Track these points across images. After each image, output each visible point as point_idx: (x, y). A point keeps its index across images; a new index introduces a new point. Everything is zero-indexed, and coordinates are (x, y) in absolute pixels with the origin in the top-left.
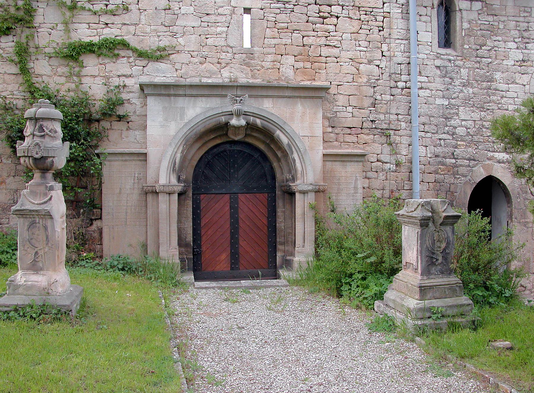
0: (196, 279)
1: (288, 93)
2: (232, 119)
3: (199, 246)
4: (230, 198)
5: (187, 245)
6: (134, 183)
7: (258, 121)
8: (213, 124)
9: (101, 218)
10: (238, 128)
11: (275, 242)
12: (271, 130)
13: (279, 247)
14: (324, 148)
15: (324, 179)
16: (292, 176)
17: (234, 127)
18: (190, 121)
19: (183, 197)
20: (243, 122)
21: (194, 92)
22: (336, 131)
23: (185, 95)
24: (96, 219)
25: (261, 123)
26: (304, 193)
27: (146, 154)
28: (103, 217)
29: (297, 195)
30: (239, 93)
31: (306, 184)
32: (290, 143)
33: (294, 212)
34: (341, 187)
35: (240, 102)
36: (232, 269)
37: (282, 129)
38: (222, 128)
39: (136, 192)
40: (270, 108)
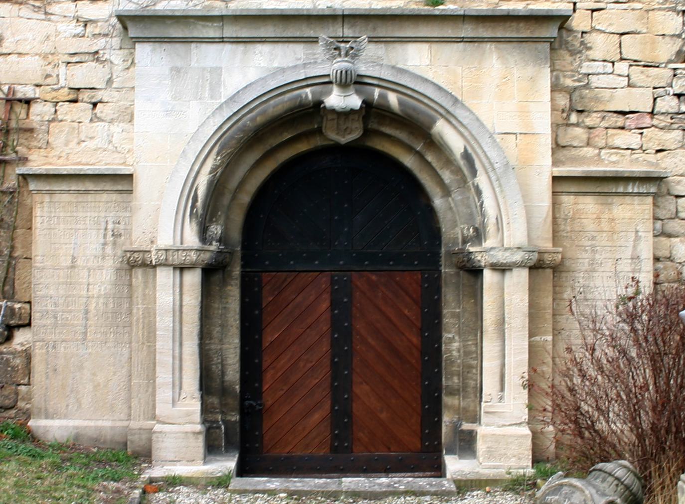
0: (243, 470)
1: (467, 31)
2: (329, 93)
3: (257, 394)
4: (333, 282)
5: (224, 391)
6: (105, 244)
7: (393, 99)
8: (287, 106)
9: (29, 325)
10: (347, 114)
11: (439, 389)
12: (422, 118)
13: (447, 400)
14: (555, 163)
15: (556, 236)
16: (476, 230)
17: (333, 111)
18: (232, 99)
19: (217, 278)
20: (355, 101)
21: (245, 32)
22: (589, 121)
23: (222, 40)
24: (19, 326)
25: (401, 103)
26: (502, 269)
27: (129, 177)
28: (33, 324)
29: (488, 276)
30: (348, 32)
31: (507, 249)
32: (470, 151)
33: (480, 318)
34: (597, 256)
35: (347, 55)
36: (334, 450)
37: (448, 117)
38: (306, 115)
39: (110, 264)
40: (421, 66)
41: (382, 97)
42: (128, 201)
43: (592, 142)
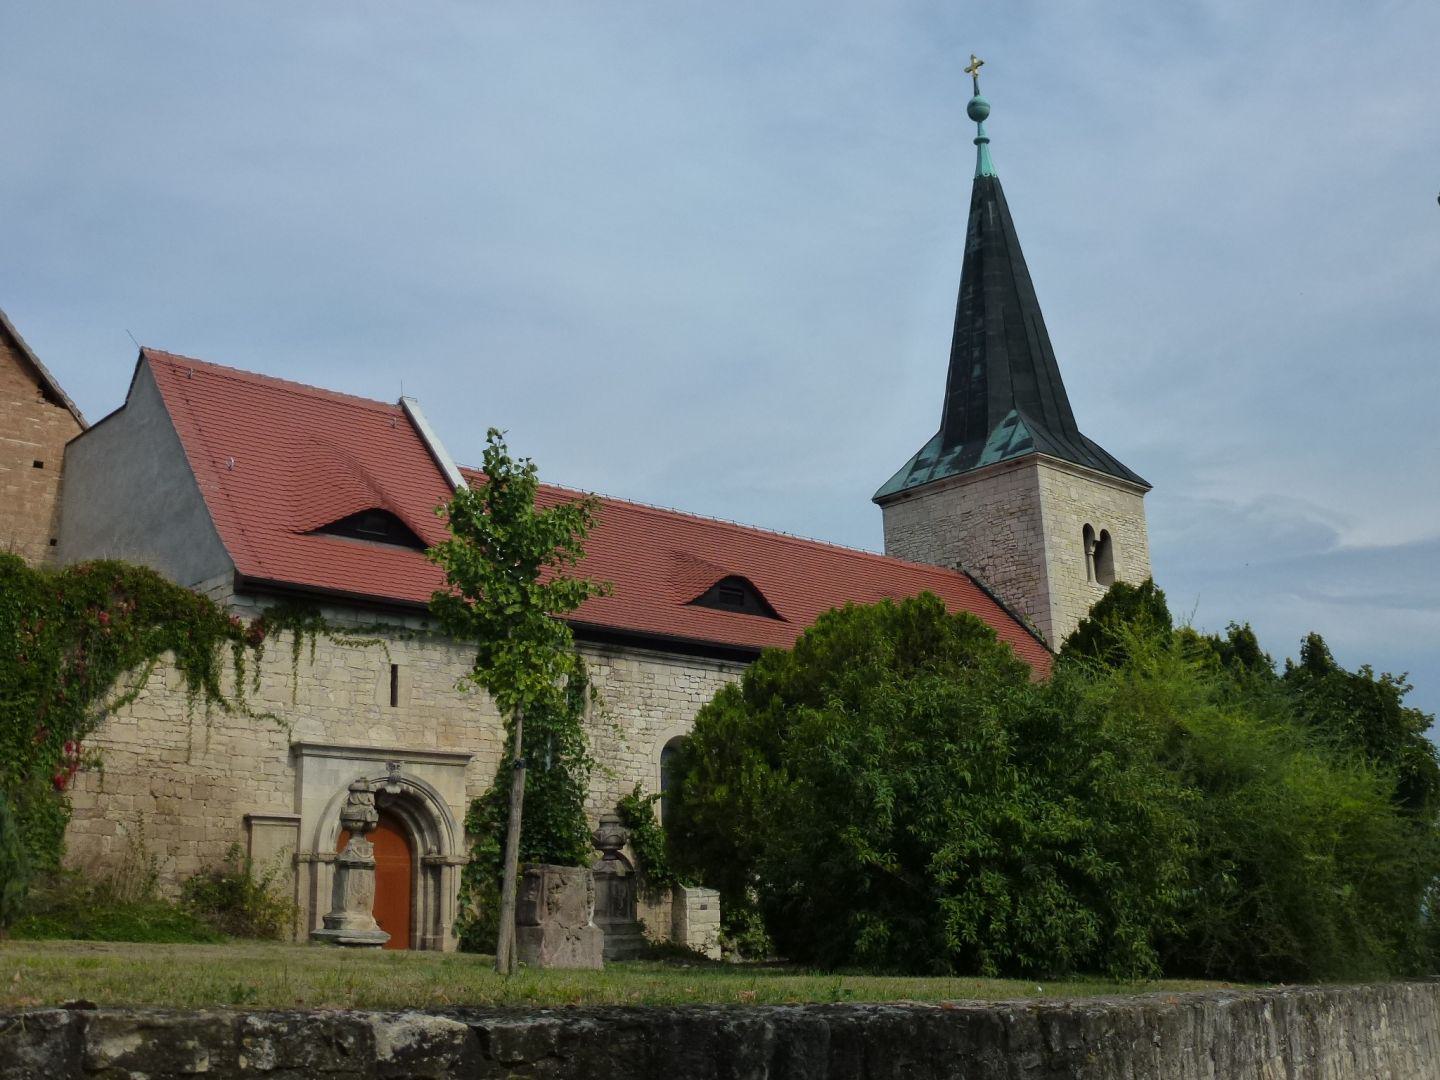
37: (433, 798)
41: (408, 788)
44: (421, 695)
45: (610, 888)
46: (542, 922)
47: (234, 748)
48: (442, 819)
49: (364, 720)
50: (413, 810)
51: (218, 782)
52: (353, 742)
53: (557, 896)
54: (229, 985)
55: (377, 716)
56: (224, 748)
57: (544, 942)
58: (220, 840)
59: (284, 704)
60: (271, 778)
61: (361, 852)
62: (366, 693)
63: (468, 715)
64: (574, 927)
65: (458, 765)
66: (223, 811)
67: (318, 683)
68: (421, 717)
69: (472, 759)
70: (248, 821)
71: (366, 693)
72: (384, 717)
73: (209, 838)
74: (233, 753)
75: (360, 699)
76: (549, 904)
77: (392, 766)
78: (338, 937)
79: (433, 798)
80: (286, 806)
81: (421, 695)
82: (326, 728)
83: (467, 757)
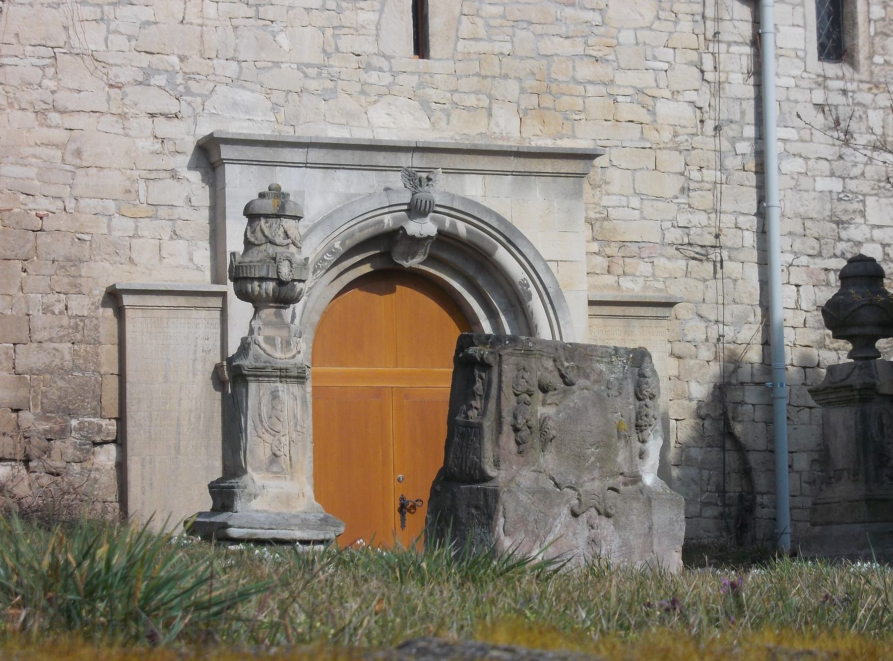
25: (469, 231)
37: (510, 244)
41: (453, 225)
42: (854, 264)
43: (611, 269)
44: (482, 32)
45: (864, 419)
46: (499, 475)
47: (78, 153)
48: (532, 289)
49: (358, 87)
50: (471, 271)
51: (47, 224)
52: (334, 133)
53: (544, 410)
54: (640, 636)
55: (387, 79)
56: (59, 154)
57: (501, 521)
58: (61, 340)
59: (182, 59)
60: (163, 212)
61: (274, 346)
62: (357, 30)
63: (586, 71)
64: (593, 484)
65: (567, 175)
66: (63, 282)
67: (251, 12)
68: (485, 77)
69: (597, 161)
70: (114, 298)
71: (357, 30)
72: (401, 79)
73: (37, 336)
74: (77, 162)
75: (346, 43)
76: (516, 430)
77: (415, 180)
78: (225, 526)
79: (510, 244)
80: (198, 269)
81: (482, 32)
82: (275, 107)
83: (589, 156)
